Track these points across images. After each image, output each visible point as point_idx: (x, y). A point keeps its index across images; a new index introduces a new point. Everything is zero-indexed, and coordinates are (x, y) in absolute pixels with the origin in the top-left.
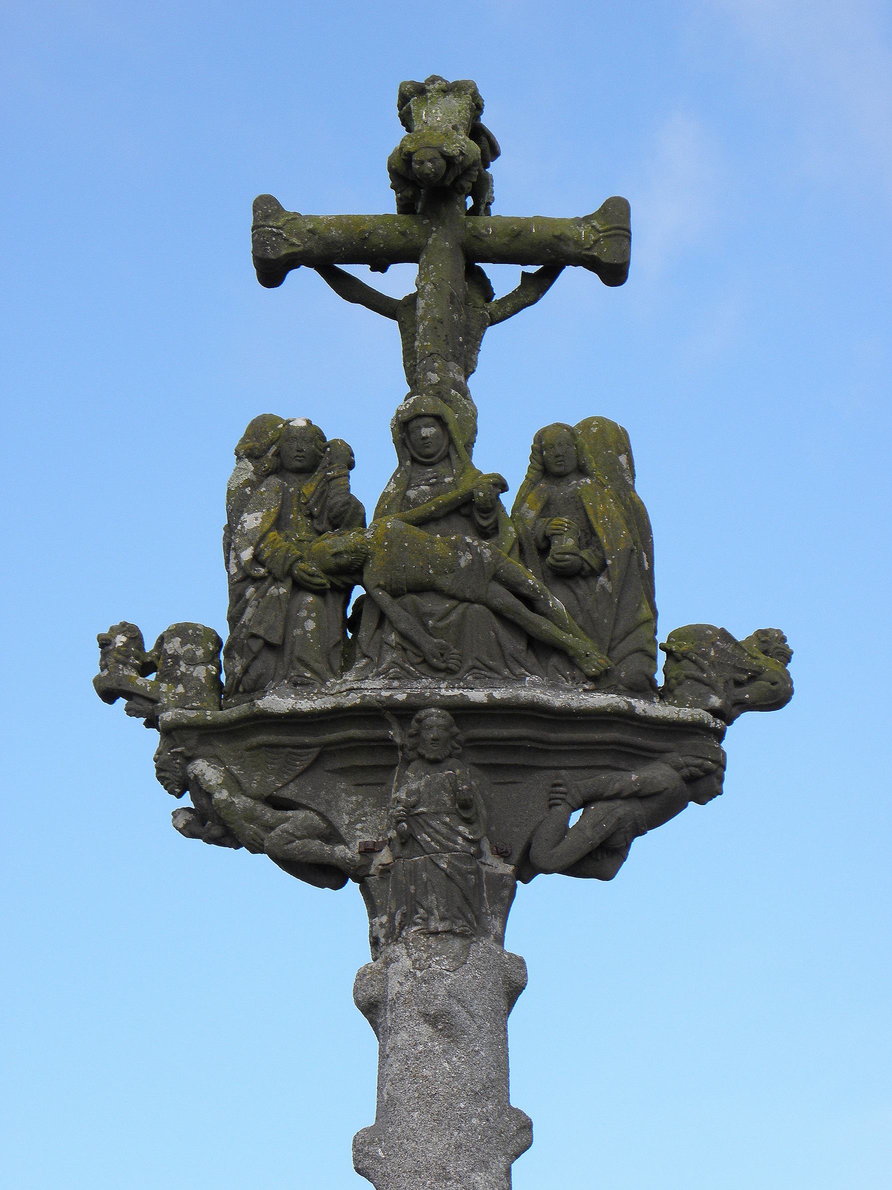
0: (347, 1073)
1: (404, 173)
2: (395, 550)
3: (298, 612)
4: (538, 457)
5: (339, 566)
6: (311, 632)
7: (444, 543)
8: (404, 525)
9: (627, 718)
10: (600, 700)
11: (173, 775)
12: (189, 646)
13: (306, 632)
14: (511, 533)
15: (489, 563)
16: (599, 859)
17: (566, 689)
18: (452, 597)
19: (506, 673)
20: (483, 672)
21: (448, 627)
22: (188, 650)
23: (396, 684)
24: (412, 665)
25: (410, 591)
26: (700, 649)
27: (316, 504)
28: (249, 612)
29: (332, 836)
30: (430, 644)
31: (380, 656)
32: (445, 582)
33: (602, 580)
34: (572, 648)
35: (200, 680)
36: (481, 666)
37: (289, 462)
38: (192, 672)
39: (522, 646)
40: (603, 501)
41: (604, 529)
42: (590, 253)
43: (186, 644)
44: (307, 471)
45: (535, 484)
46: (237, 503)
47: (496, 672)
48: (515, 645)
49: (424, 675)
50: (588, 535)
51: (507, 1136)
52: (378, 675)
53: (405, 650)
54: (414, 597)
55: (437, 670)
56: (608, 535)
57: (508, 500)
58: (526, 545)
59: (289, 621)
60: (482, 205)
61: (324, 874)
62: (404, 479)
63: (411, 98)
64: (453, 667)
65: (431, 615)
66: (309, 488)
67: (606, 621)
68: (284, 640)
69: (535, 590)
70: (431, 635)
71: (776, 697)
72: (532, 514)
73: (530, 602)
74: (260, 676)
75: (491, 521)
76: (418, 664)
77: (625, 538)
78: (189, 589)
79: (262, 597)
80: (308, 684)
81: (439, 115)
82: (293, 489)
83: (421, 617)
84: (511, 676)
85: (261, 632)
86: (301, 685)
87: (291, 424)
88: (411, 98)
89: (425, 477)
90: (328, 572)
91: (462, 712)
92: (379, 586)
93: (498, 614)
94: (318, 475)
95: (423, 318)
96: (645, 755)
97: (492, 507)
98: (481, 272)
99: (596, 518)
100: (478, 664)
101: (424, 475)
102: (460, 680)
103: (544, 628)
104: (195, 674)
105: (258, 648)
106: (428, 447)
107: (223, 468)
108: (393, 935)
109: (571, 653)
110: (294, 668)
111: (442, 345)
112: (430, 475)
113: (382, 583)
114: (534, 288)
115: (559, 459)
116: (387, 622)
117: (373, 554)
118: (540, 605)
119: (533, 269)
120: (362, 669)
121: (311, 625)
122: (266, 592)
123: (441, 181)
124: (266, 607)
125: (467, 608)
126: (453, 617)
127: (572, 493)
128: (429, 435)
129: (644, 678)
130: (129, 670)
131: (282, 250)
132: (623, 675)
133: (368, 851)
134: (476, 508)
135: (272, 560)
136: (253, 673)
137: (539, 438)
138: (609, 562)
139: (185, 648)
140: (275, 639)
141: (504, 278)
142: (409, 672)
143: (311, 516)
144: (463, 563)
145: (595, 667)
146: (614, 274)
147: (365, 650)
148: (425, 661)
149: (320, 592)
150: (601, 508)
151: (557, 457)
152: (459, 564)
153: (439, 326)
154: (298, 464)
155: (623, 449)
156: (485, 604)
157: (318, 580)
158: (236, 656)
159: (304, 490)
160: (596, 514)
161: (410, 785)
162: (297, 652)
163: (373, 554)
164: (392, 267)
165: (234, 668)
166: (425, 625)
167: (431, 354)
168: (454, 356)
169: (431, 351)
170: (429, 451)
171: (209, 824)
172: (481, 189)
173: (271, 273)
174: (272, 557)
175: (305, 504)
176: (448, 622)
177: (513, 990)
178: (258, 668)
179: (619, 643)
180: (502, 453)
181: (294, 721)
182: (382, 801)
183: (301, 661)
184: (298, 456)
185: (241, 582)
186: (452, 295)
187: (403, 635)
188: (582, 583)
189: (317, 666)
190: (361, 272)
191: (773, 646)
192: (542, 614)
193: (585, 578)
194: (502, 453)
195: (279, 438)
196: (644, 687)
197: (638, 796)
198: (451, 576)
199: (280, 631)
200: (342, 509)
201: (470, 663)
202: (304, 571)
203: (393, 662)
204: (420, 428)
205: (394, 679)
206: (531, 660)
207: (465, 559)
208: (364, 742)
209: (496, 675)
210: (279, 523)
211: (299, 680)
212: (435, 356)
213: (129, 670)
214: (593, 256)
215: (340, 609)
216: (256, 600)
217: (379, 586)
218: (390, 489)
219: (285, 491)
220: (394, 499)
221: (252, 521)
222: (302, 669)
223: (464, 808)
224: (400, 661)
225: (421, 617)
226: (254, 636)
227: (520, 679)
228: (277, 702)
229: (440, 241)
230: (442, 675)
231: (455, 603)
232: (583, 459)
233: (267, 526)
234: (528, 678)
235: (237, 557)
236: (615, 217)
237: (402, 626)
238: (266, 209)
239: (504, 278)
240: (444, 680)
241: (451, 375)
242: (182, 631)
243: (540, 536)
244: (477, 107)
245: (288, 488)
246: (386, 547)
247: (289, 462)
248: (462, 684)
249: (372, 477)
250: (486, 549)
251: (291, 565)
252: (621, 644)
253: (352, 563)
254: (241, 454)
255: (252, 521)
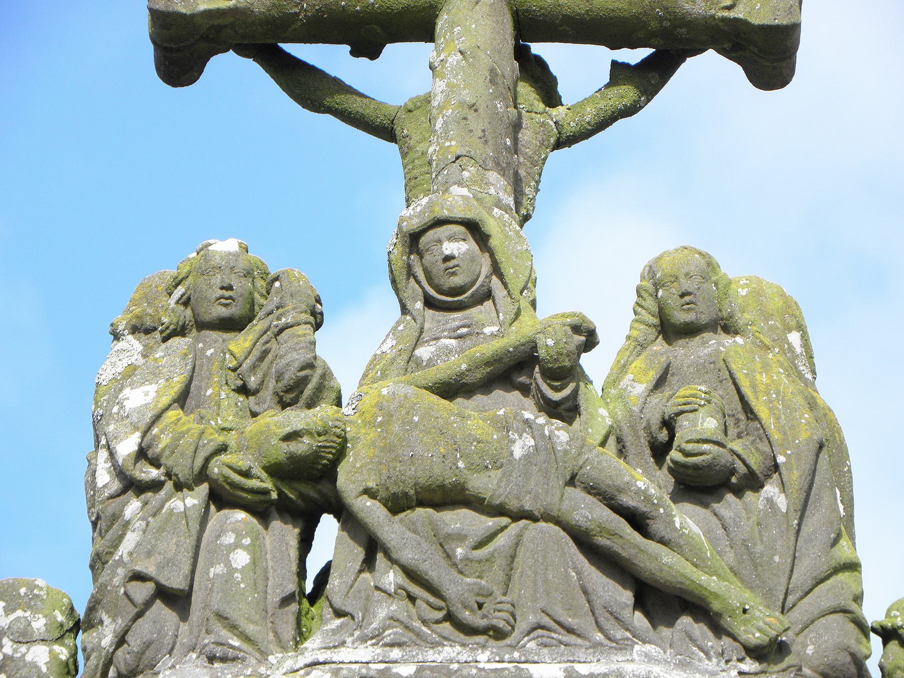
2: (396, 428)
3: (218, 537)
4: (650, 303)
5: (293, 458)
6: (242, 571)
7: (484, 420)
8: (411, 390)
12: (19, 613)
13: (231, 570)
14: (603, 418)
15: (566, 452)
17: (707, 671)
18: (499, 511)
19: (599, 636)
20: (555, 636)
21: (489, 560)
22: (18, 619)
23: (396, 653)
24: (424, 622)
25: (421, 504)
27: (254, 368)
28: (130, 541)
30: (456, 586)
31: (366, 611)
32: (484, 484)
33: (770, 489)
34: (717, 596)
35: (36, 667)
36: (552, 624)
38: (24, 655)
39: (627, 596)
40: (766, 367)
41: (770, 409)
42: (732, 14)
43: (14, 610)
45: (643, 346)
47: (579, 636)
49: (445, 638)
52: (364, 639)
53: (412, 599)
54: (430, 510)
55: (469, 630)
56: (778, 419)
57: (596, 365)
58: (629, 440)
64: (501, 624)
65: (460, 537)
66: (240, 344)
67: (777, 559)
68: (191, 586)
69: (648, 498)
70: (461, 572)
72: (641, 388)
73: (638, 521)
74: (148, 645)
75: (566, 392)
76: (438, 622)
77: (808, 423)
79: (154, 515)
80: (234, 659)
82: (212, 351)
83: (443, 542)
84: (606, 642)
85: (148, 567)
86: (224, 659)
87: (210, 248)
89: (448, 326)
90: (275, 471)
92: (367, 492)
93: (583, 540)
94: (257, 326)
95: (441, 108)
97: (566, 373)
98: (540, 63)
99: (755, 392)
100: (546, 621)
101: (447, 323)
102: (513, 647)
103: (665, 560)
104: (28, 658)
106: (454, 274)
109: (716, 606)
110: (208, 632)
112: (457, 323)
113: (371, 484)
115: (687, 299)
116: (380, 556)
117: (356, 439)
118: (656, 527)
119: (634, 56)
120: (334, 632)
121: (241, 559)
122: (162, 507)
124: (161, 530)
125: (525, 528)
126: (501, 541)
127: (710, 355)
128: (456, 254)
129: (849, 659)
132: (810, 650)
135: (173, 452)
136: (134, 641)
137: (650, 272)
138: (781, 459)
139: (12, 617)
140: (176, 581)
141: (581, 69)
142: (418, 635)
143: (244, 390)
144: (518, 451)
145: (760, 630)
147: (338, 602)
148: (450, 617)
149: (262, 510)
150: (764, 378)
151: (682, 296)
152: (512, 454)
153: (471, 115)
154: (221, 311)
155: (793, 323)
156: (557, 522)
157: (253, 483)
158: (105, 617)
159: (232, 347)
160: (754, 386)
162: (216, 602)
163: (356, 439)
164: (391, 49)
165: (100, 640)
166: (449, 556)
167: (458, 158)
168: (497, 164)
169: (459, 153)
170: (456, 281)
174: (173, 448)
175: (234, 370)
176: (491, 549)
178: (143, 630)
179: (802, 598)
183: (221, 617)
184: (222, 297)
186: (492, 71)
187: (411, 574)
188: (730, 497)
189: (251, 629)
192: (662, 541)
193: (738, 492)
195: (189, 273)
198: (496, 474)
199: (186, 568)
200: (302, 373)
201: (532, 619)
202: (231, 467)
203: (392, 618)
204: (440, 241)
205: (392, 645)
206: (639, 619)
207: (522, 445)
209: (579, 641)
211: (219, 651)
212: (465, 159)
214: (737, 20)
215: (294, 553)
216: (143, 519)
217: (367, 492)
218: (385, 348)
219: (198, 356)
220: (393, 360)
222: (225, 634)
224: (403, 616)
225: (443, 542)
226: (138, 577)
227: (622, 646)
230: (481, 639)
231: (505, 520)
233: (165, 400)
234: (637, 647)
235: (112, 455)
237: (408, 556)
240: (484, 647)
241: (492, 191)
243: (656, 421)
245: (203, 350)
246: (381, 424)
248: (516, 655)
250: (560, 432)
251: (207, 460)
252: (806, 600)
253: (316, 456)
254: (121, 328)
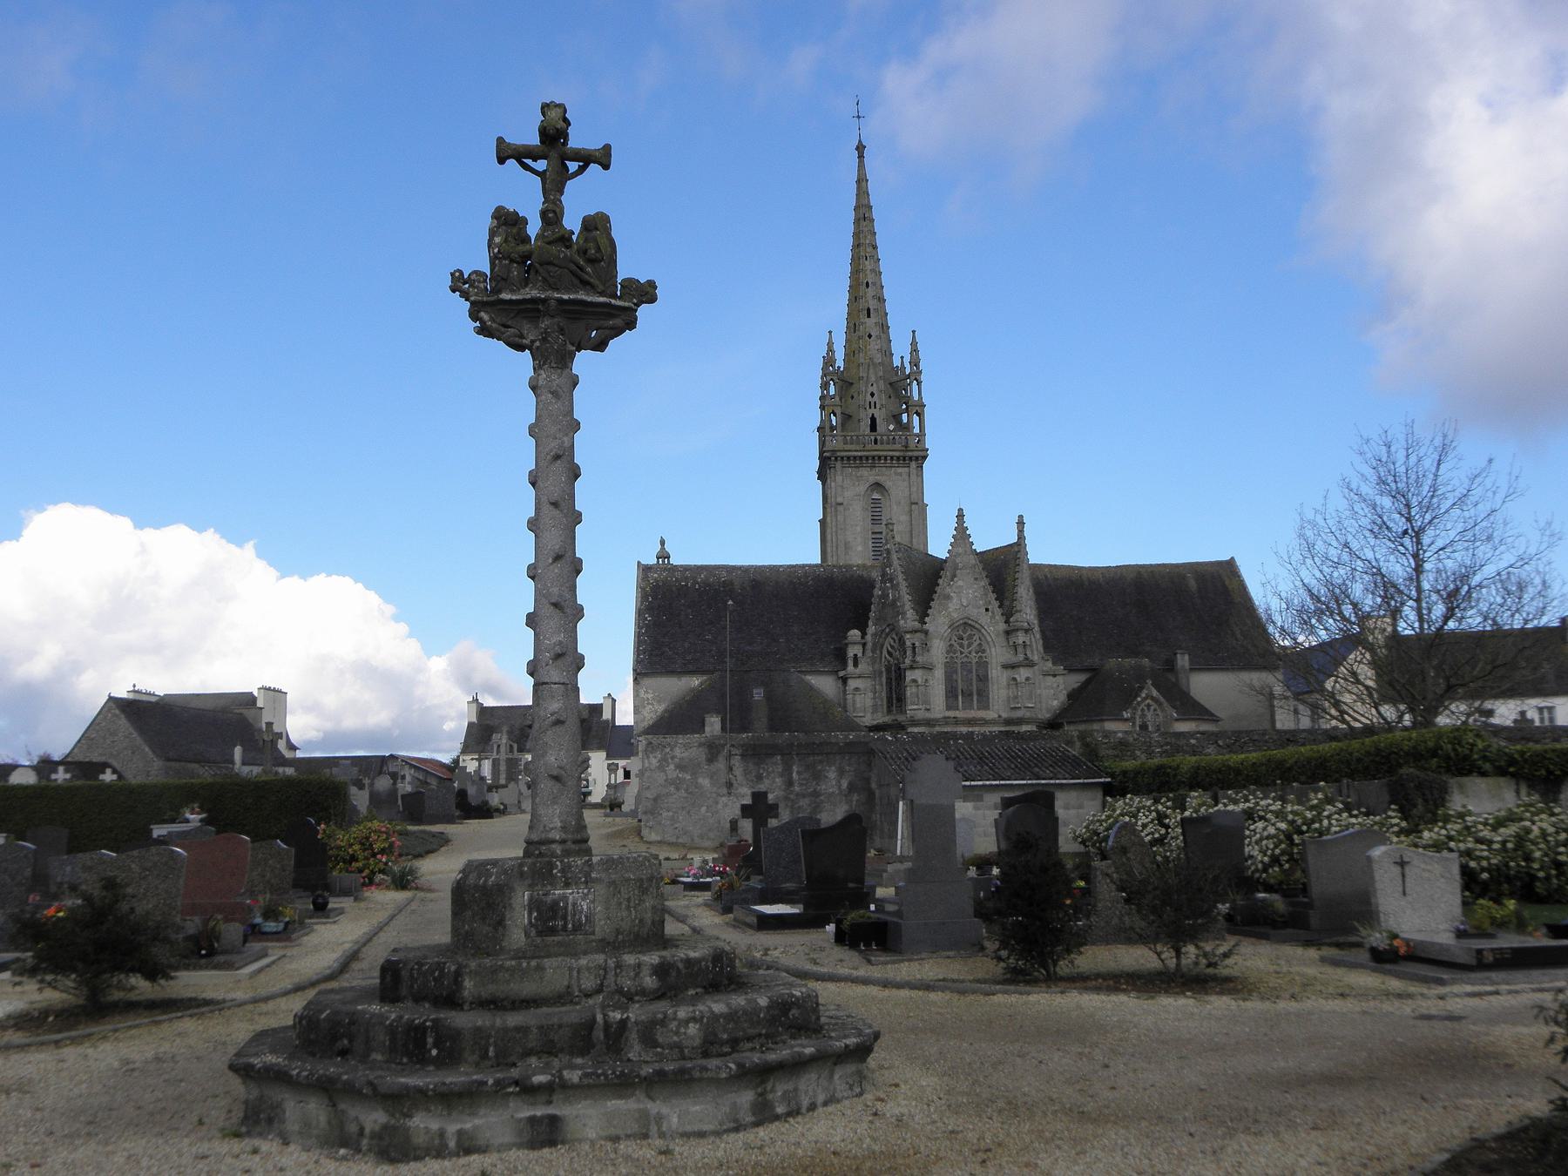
0: (526, 407)
1: (543, 132)
9: (609, 305)
10: (602, 299)
11: (474, 315)
16: (600, 346)
26: (630, 284)
29: (522, 336)
30: (551, 280)
37: (507, 221)
44: (514, 225)
46: (492, 233)
48: (576, 282)
50: (598, 249)
51: (1265, 829)
57: (574, 238)
59: (509, 271)
60: (565, 143)
61: (519, 347)
62: (543, 229)
63: (545, 107)
71: (653, 300)
78: (479, 261)
81: (554, 114)
88: (545, 107)
91: (561, 301)
96: (612, 316)
105: (500, 279)
107: (487, 222)
108: (540, 367)
111: (554, 185)
114: (581, 170)
123: (553, 136)
130: (460, 283)
131: (506, 153)
133: (533, 342)
134: (565, 239)
141: (573, 166)
146: (606, 167)
161: (545, 323)
171: (483, 331)
172: (566, 137)
173: (501, 160)
177: (575, 384)
180: (572, 222)
181: (511, 301)
182: (537, 327)
185: (493, 260)
190: (529, 161)
191: (652, 285)
194: (572, 222)
196: (614, 296)
197: (612, 328)
208: (531, 310)
210: (506, 241)
213: (460, 283)
221: (497, 240)
223: (562, 331)
228: (505, 296)
229: (553, 154)
232: (596, 225)
236: (607, 149)
238: (500, 141)
239: (573, 166)
242: (475, 272)
244: (565, 111)
247: (507, 221)
249: (534, 228)
255: (497, 240)
